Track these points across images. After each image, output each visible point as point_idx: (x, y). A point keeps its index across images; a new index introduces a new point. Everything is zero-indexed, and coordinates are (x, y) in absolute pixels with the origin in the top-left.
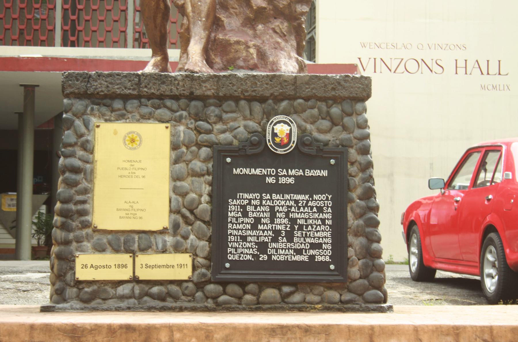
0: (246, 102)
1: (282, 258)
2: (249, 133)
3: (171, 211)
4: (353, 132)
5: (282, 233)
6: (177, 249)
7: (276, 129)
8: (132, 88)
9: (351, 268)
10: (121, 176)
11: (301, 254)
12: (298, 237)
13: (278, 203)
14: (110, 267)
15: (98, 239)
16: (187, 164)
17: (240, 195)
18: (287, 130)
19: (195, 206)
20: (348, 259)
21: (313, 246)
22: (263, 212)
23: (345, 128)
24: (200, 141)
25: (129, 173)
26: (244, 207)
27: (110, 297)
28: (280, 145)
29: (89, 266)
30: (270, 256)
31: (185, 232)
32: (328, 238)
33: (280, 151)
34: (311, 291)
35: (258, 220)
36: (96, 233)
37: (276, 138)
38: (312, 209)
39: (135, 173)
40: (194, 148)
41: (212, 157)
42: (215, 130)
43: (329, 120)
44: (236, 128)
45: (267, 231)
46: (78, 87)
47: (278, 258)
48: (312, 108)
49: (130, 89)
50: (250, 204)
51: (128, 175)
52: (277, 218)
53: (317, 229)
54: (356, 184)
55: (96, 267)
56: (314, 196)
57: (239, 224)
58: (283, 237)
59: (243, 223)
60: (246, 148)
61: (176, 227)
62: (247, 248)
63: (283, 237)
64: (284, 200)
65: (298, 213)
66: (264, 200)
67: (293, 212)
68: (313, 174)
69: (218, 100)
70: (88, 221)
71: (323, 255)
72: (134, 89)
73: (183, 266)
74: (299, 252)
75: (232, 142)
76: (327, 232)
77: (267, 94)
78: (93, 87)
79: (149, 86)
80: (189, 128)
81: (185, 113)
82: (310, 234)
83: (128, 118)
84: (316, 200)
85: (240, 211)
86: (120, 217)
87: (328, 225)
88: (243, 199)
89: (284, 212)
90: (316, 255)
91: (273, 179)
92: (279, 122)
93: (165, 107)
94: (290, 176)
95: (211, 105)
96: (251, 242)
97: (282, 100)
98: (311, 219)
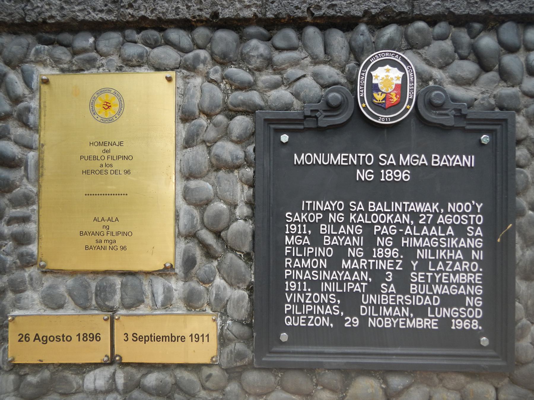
0: (317, 30)
1: (387, 324)
2: (324, 86)
3: (178, 235)
4: (520, 84)
5: (387, 276)
6: (191, 302)
7: (377, 77)
8: (105, 8)
9: (519, 340)
10: (87, 172)
11: (424, 315)
12: (417, 283)
13: (379, 218)
14: (69, 339)
15: (50, 287)
16: (208, 147)
17: (306, 204)
18: (398, 78)
19: (222, 225)
20: (516, 323)
21: (448, 301)
22: (350, 235)
23: (505, 76)
24: (231, 103)
25: (102, 166)
26: (314, 227)
27: (74, 391)
28: (381, 108)
29: (32, 338)
30: (364, 320)
31: (205, 272)
32: (476, 285)
33: (383, 119)
34: (441, 380)
35: (341, 252)
36: (48, 275)
37: (375, 95)
38: (444, 230)
39: (111, 165)
40: (220, 118)
41: (253, 134)
42: (260, 84)
43: (474, 61)
44: (299, 79)
45: (359, 271)
46: (9, 11)
47: (380, 322)
48: (442, 38)
49: (101, 11)
50: (325, 220)
51: (100, 169)
52: (377, 248)
53: (455, 269)
54: (528, 181)
55: (45, 340)
56: (450, 205)
57: (306, 259)
58: (389, 284)
59: (312, 256)
60: (317, 114)
61: (189, 263)
62: (320, 304)
63: (389, 284)
64: (390, 213)
65: (418, 238)
66: (353, 213)
67: (409, 235)
68: (447, 163)
69: (265, 27)
70: (32, 255)
71: (467, 318)
72: (110, 11)
73: (201, 338)
74: (419, 311)
75: (292, 104)
76: (475, 273)
77: (357, 11)
78: (36, 10)
79: (136, 5)
80: (211, 81)
81: (203, 54)
82: (441, 278)
83: (103, 65)
84: (452, 213)
85: (307, 234)
86: (86, 247)
87: (475, 260)
88: (311, 210)
89: (390, 235)
90: (452, 318)
91: (370, 173)
92: (382, 63)
93: (168, 43)
94: (402, 168)
95: (252, 37)
96: (328, 292)
97: (385, 24)
98: (443, 249)
